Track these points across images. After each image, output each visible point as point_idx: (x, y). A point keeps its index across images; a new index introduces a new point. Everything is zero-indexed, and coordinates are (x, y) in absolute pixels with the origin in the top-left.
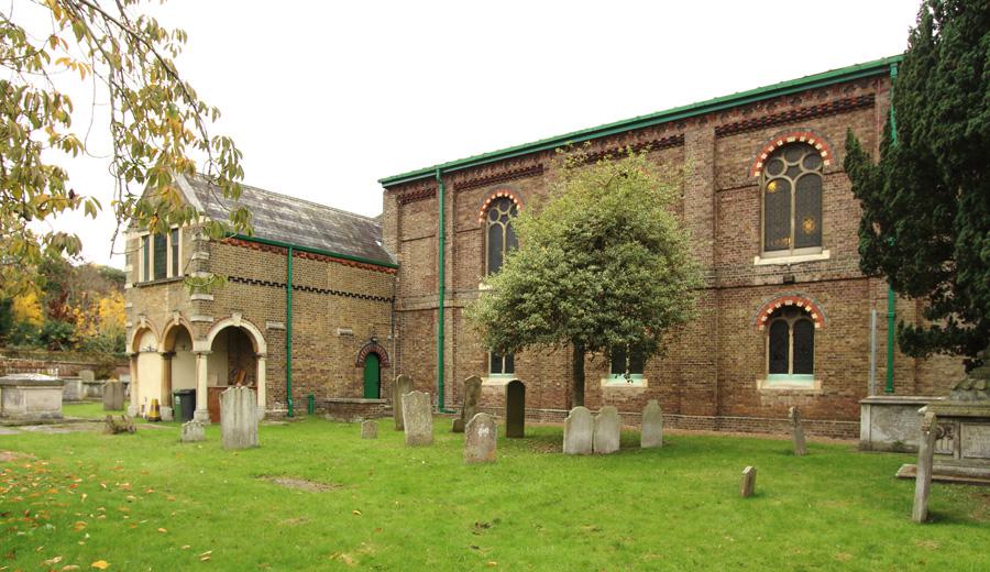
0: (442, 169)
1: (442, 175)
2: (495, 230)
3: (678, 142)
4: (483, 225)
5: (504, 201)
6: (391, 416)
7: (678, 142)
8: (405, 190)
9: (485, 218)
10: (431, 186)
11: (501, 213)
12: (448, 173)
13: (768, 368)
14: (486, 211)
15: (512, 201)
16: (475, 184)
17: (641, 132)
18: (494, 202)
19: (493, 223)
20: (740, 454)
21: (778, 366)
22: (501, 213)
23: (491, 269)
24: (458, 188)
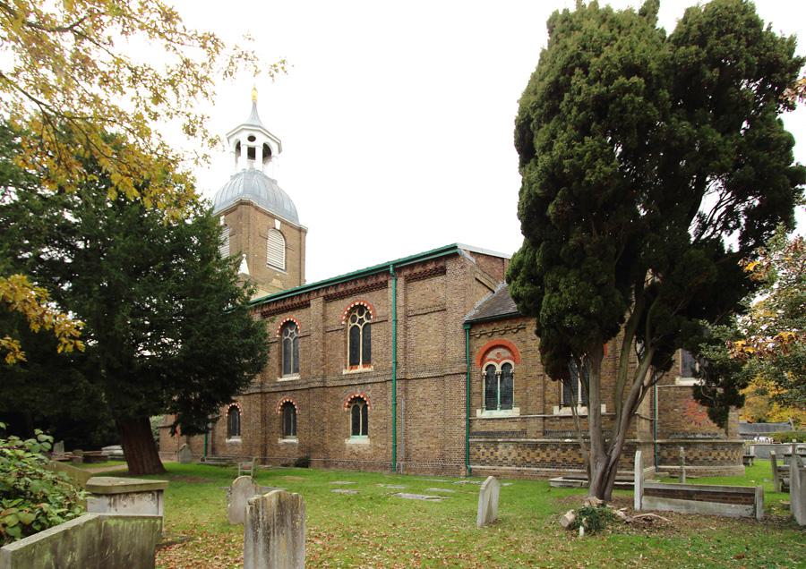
0: (394, 265)
1: (395, 270)
2: (355, 329)
3: (443, 271)
4: (281, 339)
5: (361, 309)
6: (249, 474)
7: (443, 271)
8: (356, 283)
9: (347, 321)
10: (382, 279)
11: (290, 331)
12: (400, 267)
13: (351, 431)
14: (348, 316)
15: (366, 308)
16: (341, 296)
17: (412, 267)
18: (353, 309)
19: (353, 325)
20: (262, 477)
21: (356, 432)
22: (359, 317)
23: (351, 364)
24: (408, 280)
